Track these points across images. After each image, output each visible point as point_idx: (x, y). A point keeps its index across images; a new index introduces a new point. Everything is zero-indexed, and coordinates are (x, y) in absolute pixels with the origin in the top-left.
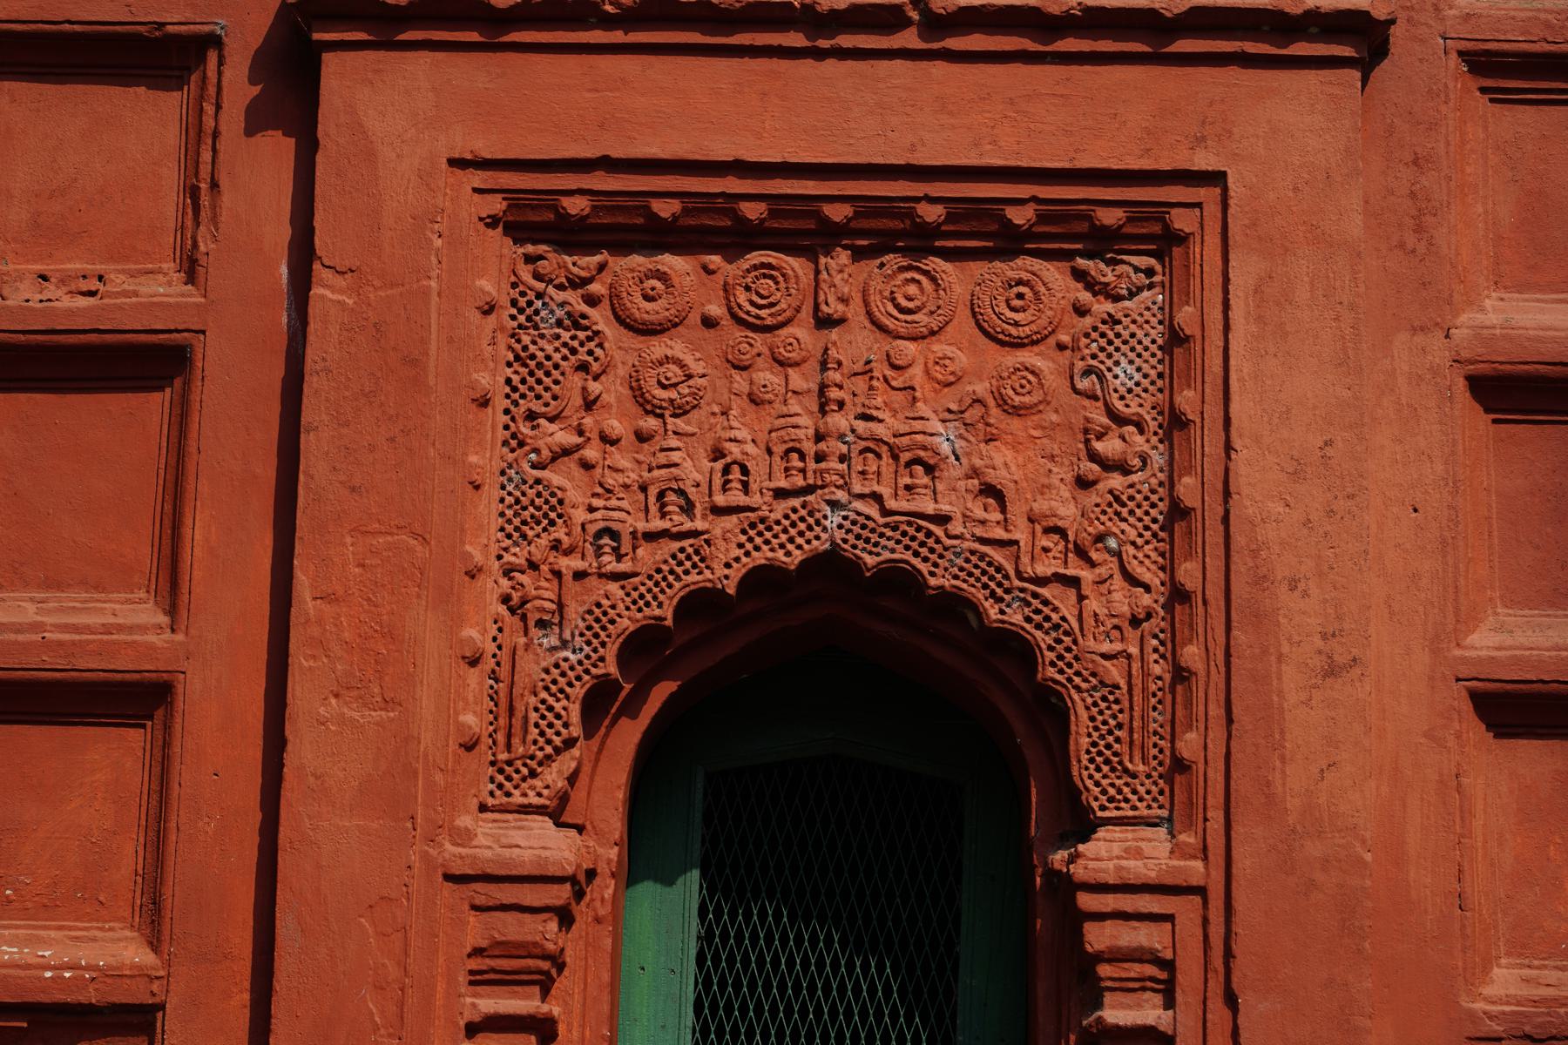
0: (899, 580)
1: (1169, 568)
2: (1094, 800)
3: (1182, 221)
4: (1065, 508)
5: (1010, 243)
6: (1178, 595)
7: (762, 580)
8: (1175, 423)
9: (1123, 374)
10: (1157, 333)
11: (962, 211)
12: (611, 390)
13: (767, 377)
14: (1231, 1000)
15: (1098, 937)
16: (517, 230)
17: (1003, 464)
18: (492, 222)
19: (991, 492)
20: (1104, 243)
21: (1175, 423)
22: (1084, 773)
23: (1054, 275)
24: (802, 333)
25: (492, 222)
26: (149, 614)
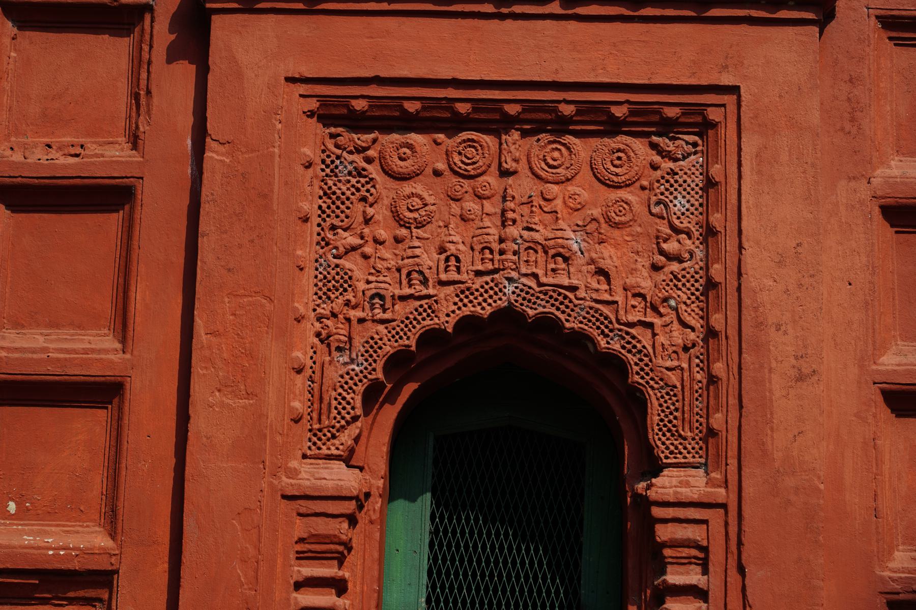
0: (548, 324)
1: (706, 317)
2: (662, 453)
3: (714, 115)
4: (645, 282)
5: (613, 127)
6: (711, 333)
7: (467, 324)
8: (710, 233)
9: (679, 204)
10: (699, 180)
11: (637, 110)
12: (380, 212)
13: (471, 205)
14: (741, 570)
15: (663, 533)
16: (326, 119)
17: (609, 256)
18: (311, 114)
19: (602, 273)
20: (668, 127)
21: (710, 233)
22: (656, 437)
23: (639, 146)
24: (491, 180)
25: (311, 114)
26: (110, 343)
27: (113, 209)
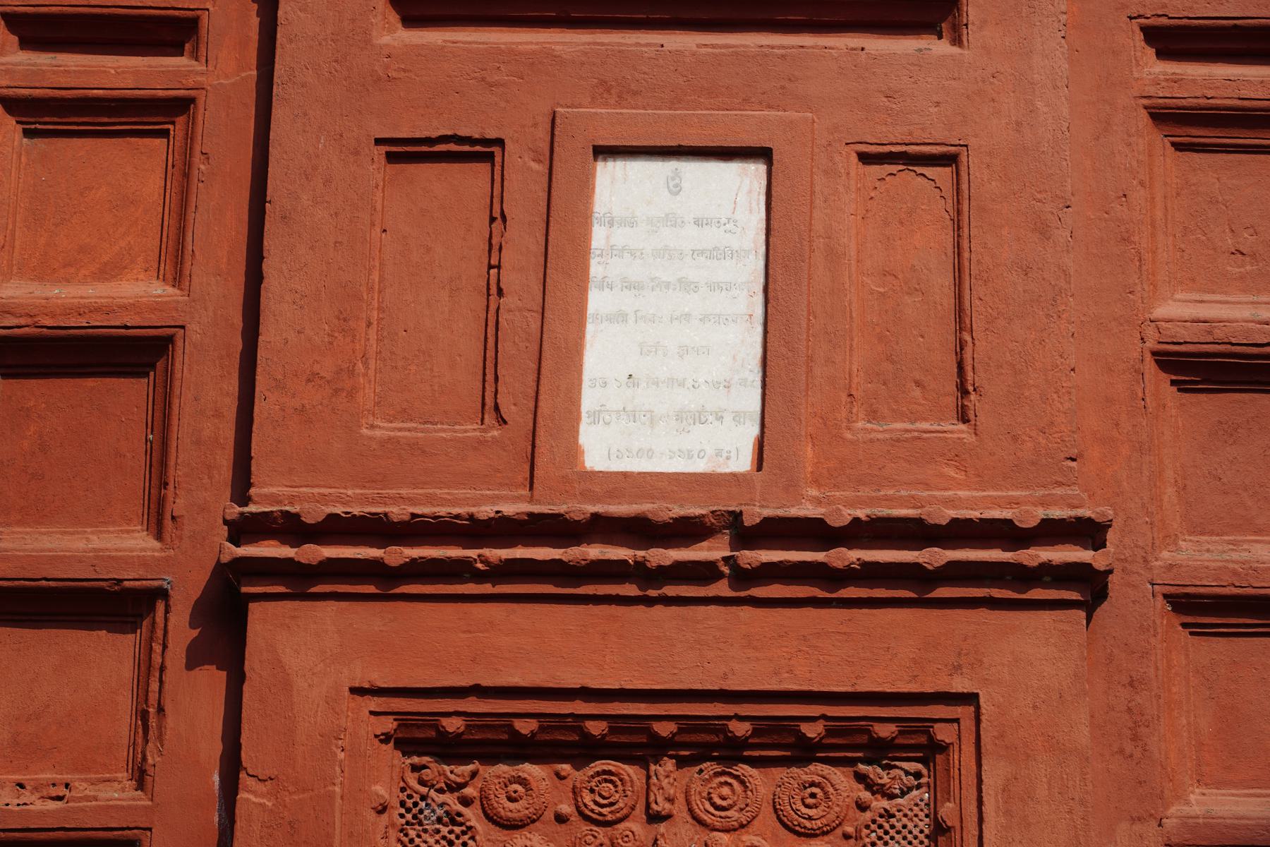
3: (943, 733)
5: (804, 753)
11: (765, 727)
16: (406, 745)
18: (385, 738)
20: (881, 752)
23: (840, 778)
25: (385, 738)
27: (133, 627)
